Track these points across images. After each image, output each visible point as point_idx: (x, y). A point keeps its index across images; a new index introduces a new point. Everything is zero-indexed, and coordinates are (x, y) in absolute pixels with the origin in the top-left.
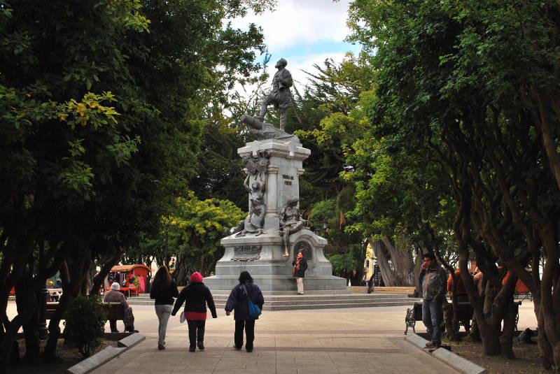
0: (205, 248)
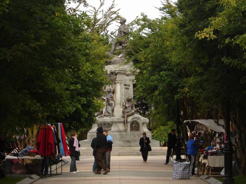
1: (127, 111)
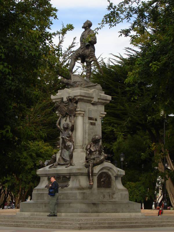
1: (93, 157)
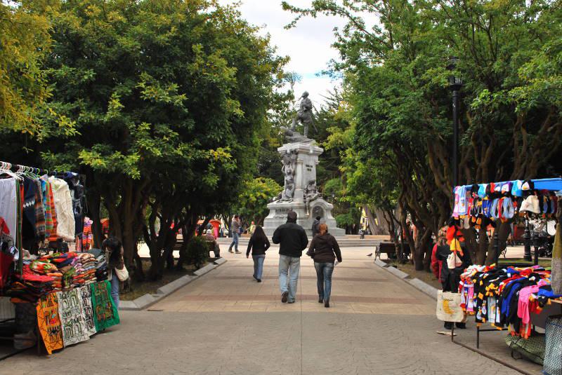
0: (256, 209)
1: (309, 195)
